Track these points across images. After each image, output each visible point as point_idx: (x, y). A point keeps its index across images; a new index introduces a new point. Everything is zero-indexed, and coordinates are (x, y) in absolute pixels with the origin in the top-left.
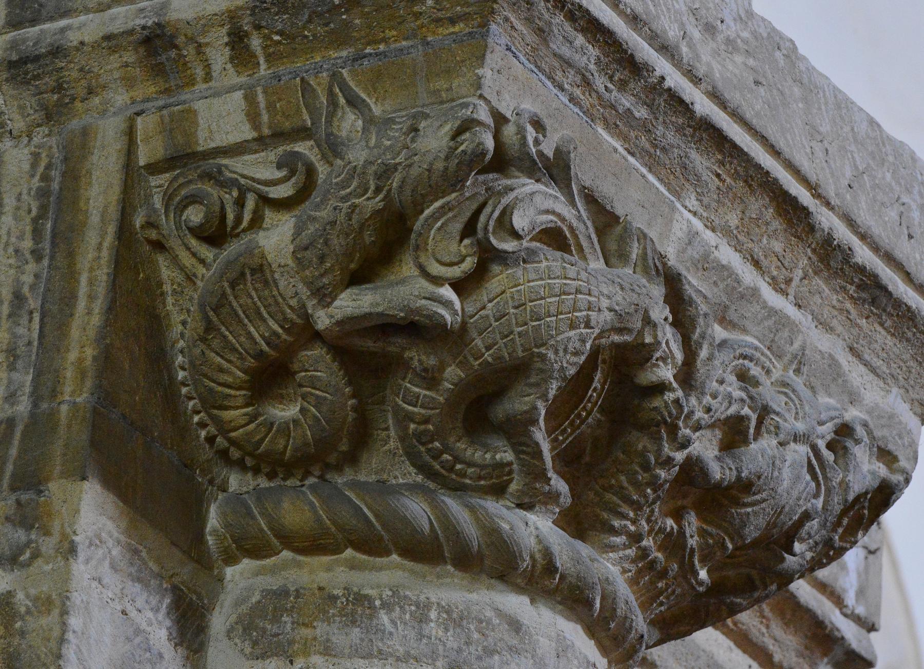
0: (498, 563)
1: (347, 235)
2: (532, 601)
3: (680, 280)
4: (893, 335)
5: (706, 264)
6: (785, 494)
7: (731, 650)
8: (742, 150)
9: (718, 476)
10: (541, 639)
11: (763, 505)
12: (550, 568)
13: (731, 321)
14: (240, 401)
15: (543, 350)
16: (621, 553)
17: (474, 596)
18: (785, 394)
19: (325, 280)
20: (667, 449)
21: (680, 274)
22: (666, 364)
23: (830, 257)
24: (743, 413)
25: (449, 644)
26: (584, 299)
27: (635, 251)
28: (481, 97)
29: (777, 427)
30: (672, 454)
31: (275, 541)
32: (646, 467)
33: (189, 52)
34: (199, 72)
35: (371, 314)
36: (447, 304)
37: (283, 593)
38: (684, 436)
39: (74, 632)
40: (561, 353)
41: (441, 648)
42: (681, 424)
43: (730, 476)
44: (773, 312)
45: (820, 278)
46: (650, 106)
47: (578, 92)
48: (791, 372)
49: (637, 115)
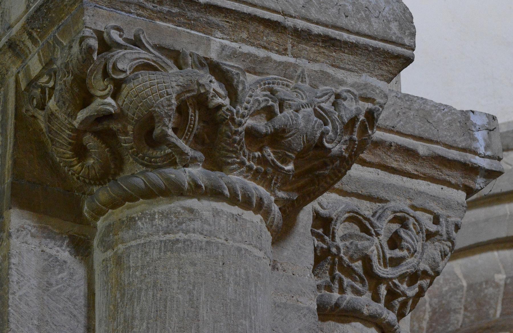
0: (175, 190)
1: (68, 92)
2: (199, 200)
3: (219, 65)
4: (352, 55)
5: (234, 55)
6: (304, 129)
7: (429, 185)
8: (232, 10)
9: (264, 131)
10: (204, 212)
11: (295, 135)
12: (198, 186)
13: (259, 73)
14: (76, 162)
15: (153, 109)
16: (239, 171)
17: (172, 205)
18: (296, 91)
19: (69, 110)
20: (233, 128)
21: (218, 63)
22: (216, 98)
23: (302, 36)
24: (269, 104)
25: (164, 225)
26: (168, 85)
27: (190, 60)
28: (86, 27)
29: (290, 105)
30: (236, 129)
31: (104, 208)
32: (229, 137)
33: (21, 45)
34: (28, 51)
35: (87, 117)
36: (109, 104)
37: (110, 225)
38: (238, 121)
39: (14, 264)
40: (162, 108)
41: (160, 228)
42: (235, 117)
43: (270, 130)
44: (280, 63)
45: (302, 44)
46: (178, 6)
47: (140, 12)
48: (300, 82)
49: (173, 11)
